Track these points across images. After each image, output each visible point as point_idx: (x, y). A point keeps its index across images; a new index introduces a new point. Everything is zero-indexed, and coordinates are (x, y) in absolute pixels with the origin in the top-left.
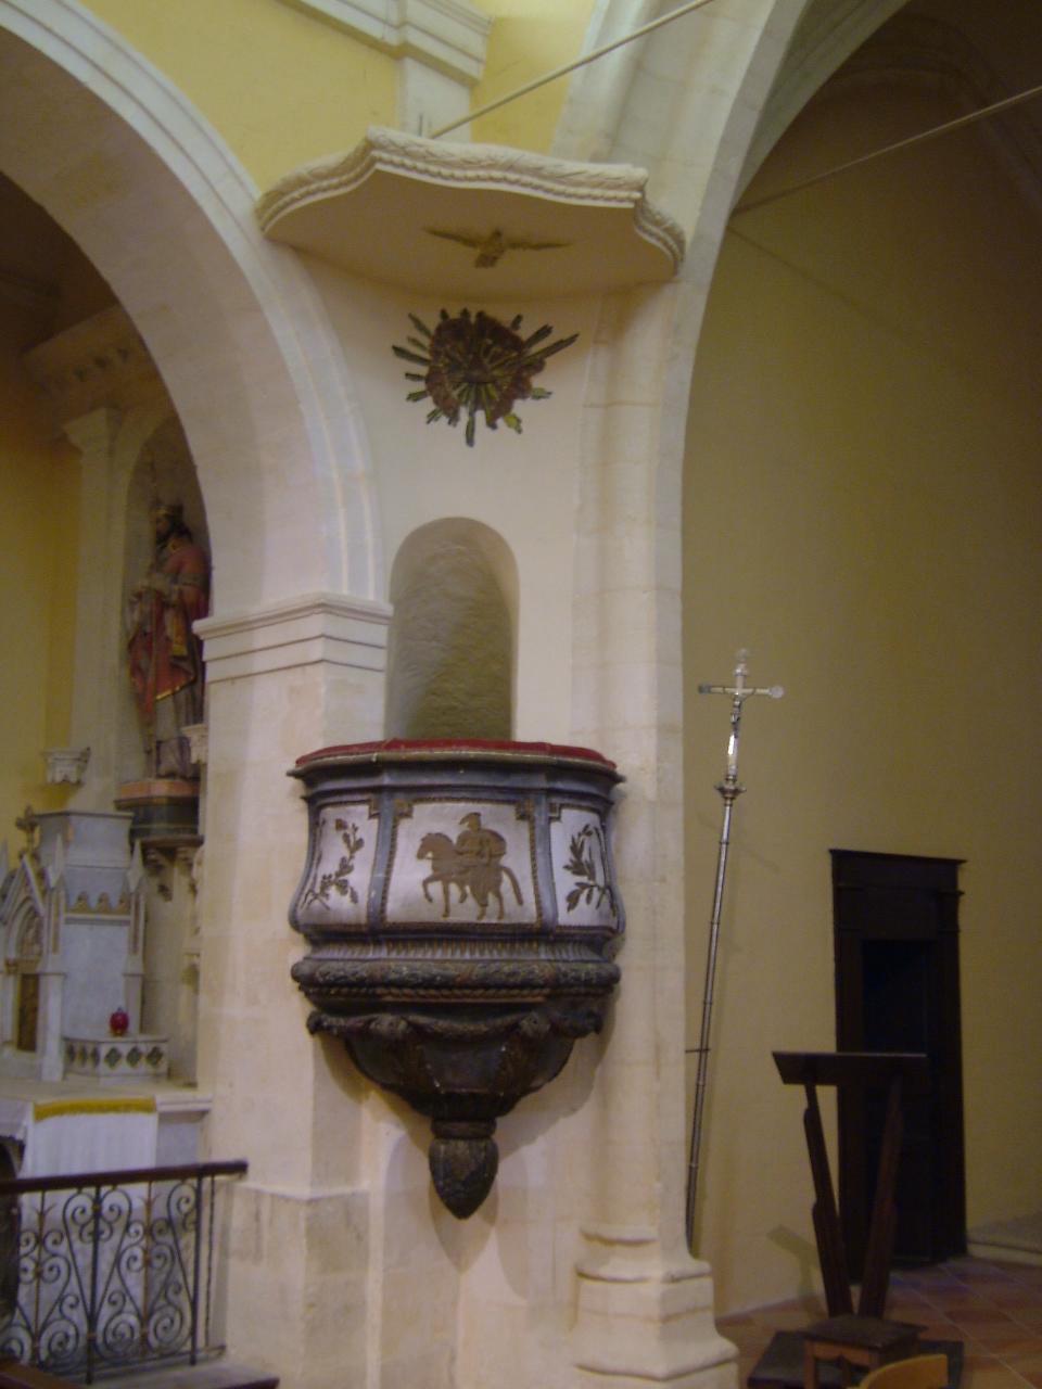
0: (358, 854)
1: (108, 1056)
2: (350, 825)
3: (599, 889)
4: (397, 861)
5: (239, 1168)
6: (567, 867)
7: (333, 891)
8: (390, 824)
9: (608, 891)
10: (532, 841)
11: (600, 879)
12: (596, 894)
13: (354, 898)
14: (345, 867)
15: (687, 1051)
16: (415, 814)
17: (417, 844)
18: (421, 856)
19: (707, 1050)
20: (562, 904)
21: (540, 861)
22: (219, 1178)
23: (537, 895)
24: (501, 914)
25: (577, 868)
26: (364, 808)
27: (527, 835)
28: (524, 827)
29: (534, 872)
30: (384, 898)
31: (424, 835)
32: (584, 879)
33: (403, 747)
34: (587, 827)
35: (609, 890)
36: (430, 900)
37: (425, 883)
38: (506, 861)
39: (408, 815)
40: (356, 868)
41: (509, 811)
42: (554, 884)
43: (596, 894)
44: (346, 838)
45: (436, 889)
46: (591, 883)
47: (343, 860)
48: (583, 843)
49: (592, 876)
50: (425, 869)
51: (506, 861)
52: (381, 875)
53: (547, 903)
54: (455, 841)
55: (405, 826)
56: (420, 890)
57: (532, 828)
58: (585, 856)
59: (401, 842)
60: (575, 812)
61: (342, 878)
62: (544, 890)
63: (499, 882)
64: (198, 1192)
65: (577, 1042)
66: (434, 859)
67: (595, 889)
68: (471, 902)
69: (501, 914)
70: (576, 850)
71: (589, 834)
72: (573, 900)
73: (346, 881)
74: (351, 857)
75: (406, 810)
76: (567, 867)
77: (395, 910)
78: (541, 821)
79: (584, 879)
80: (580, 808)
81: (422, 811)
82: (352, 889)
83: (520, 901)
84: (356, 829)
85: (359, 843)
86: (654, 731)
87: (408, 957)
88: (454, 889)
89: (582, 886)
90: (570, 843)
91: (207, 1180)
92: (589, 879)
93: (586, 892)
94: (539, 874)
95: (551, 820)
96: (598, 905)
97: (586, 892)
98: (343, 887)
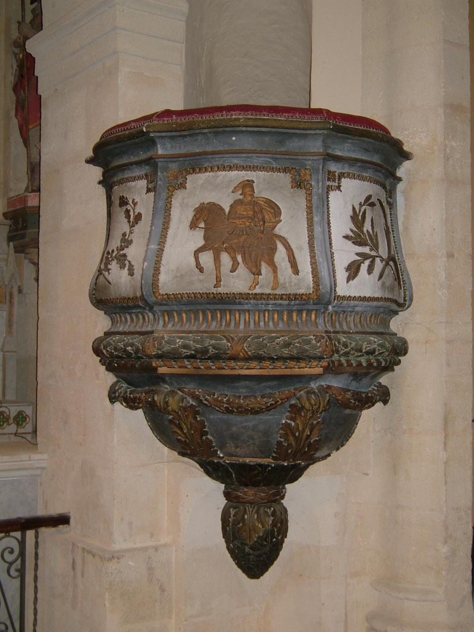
0: (136, 229)
1: (15, 418)
2: (131, 202)
3: (382, 260)
4: (170, 233)
5: (63, 520)
6: (346, 237)
7: (114, 266)
8: (164, 195)
9: (391, 263)
10: (310, 209)
11: (383, 251)
12: (379, 265)
13: (131, 274)
14: (126, 242)
15: (37, 445)
16: (40, 94)
17: (190, 215)
18: (193, 225)
19: (15, 436)
20: (341, 275)
21: (317, 229)
22: (45, 531)
23: (314, 264)
24: (276, 284)
25: (357, 239)
26: (143, 183)
27: (303, 203)
28: (301, 195)
29: (311, 238)
30: (157, 271)
31: (197, 206)
32: (366, 250)
33: (188, 137)
34: (369, 197)
35: (393, 261)
36: (201, 270)
37: (197, 253)
38: (281, 229)
39: (183, 186)
40: (134, 241)
41: (285, 179)
42: (332, 254)
43: (379, 265)
44: (128, 216)
45: (207, 259)
46: (373, 253)
47: (124, 235)
48: (364, 213)
49: (375, 247)
50: (197, 239)
51: (281, 229)
52: (154, 247)
53: (324, 273)
54: (227, 210)
55: (178, 199)
56: (192, 259)
57: (309, 195)
58: (367, 226)
59: (175, 213)
60: (356, 182)
61: (122, 252)
62: (320, 259)
63: (274, 250)
64: (22, 543)
65: (365, 413)
66: (206, 229)
67: (378, 260)
68: (242, 269)
69: (275, 286)
70: (357, 219)
71: (372, 205)
72: (353, 270)
73: (125, 255)
74: (131, 233)
75: (39, 97)
76: (346, 237)
77: (167, 283)
78: (317, 188)
79: (366, 250)
80: (362, 179)
81: (195, 181)
82: (129, 262)
83: (296, 270)
84: (135, 204)
85: (138, 217)
86: (441, 111)
87: (183, 329)
88: (225, 258)
89: (364, 256)
90: (351, 213)
91: (30, 534)
92: (371, 250)
93: (367, 262)
94: (317, 244)
95: (329, 189)
96: (381, 277)
97: (367, 262)
98: (122, 259)
